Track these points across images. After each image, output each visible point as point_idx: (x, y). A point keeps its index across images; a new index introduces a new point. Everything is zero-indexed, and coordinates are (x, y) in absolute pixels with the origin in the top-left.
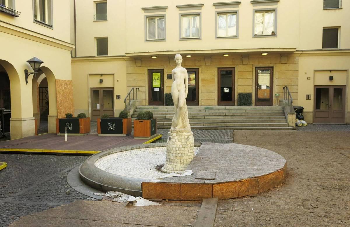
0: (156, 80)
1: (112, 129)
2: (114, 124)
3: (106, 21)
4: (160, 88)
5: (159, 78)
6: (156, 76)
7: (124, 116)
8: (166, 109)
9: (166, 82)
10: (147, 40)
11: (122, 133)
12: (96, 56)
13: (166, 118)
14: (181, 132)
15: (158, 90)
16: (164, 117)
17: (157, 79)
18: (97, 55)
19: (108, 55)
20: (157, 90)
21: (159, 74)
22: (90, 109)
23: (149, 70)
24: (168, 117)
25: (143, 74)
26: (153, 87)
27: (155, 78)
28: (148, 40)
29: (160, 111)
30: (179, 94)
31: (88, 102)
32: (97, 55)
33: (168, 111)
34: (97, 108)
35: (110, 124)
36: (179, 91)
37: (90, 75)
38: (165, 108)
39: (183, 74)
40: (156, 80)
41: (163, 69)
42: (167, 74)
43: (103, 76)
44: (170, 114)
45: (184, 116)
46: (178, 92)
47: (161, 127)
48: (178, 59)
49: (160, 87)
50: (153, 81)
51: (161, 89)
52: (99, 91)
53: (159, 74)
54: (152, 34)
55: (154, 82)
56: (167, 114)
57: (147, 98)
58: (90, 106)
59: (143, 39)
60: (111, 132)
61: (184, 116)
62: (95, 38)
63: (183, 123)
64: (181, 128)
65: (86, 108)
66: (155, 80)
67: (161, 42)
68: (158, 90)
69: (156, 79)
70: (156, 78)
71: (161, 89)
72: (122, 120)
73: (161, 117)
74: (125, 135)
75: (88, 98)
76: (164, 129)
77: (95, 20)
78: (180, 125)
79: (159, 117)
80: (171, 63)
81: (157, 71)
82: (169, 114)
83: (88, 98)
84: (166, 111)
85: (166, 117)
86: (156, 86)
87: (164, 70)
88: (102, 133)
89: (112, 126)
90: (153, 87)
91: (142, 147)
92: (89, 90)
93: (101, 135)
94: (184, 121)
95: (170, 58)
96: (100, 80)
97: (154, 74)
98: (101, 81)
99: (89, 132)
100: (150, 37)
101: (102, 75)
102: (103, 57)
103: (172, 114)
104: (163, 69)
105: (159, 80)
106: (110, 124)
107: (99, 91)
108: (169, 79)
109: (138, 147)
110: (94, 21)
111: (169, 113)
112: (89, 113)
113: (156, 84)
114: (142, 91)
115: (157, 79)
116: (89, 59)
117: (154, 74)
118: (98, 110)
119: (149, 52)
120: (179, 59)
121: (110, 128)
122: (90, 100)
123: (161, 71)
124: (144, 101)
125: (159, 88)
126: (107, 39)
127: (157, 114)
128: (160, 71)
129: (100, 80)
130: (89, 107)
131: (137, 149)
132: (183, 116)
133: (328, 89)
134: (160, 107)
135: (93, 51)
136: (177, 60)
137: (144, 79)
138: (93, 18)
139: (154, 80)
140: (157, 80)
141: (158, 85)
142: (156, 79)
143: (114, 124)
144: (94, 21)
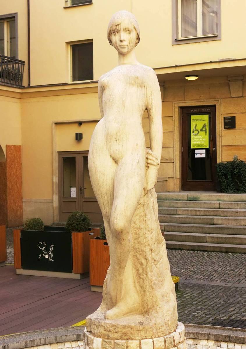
0: (199, 132)
1: (48, 259)
2: (52, 246)
3: (91, 4)
4: (207, 150)
5: (205, 126)
6: (199, 122)
7: (77, 225)
8: (218, 200)
9: (221, 136)
10: (177, 41)
11: (70, 272)
12: (69, 80)
13: (213, 224)
14: (125, 334)
15: (204, 156)
16: (209, 221)
17: (201, 130)
18: (73, 81)
19: (93, 79)
20: (200, 154)
21: (206, 117)
22: (56, 198)
23: (182, 108)
24: (220, 222)
25: (169, 119)
26: (192, 147)
27: (196, 126)
28: (180, 39)
29: (202, 206)
30: (116, 173)
31: (53, 182)
32: (73, 81)
33: (222, 206)
34: (71, 197)
35: (42, 245)
36: (116, 161)
37: (57, 124)
38: (215, 199)
39: (134, 90)
40: (199, 132)
41: (214, 106)
42: (224, 117)
43: (83, 126)
44: (225, 214)
45: (144, 261)
46: (114, 164)
47: (198, 246)
48: (118, 31)
49: (208, 147)
50: (192, 134)
51: (211, 152)
52: (75, 158)
53: (206, 117)
54: (189, 22)
55: (193, 137)
56: (218, 214)
57: (178, 175)
58: (56, 190)
59: (169, 38)
60: (44, 265)
61: (144, 261)
62: (68, 43)
63: (142, 291)
64: (131, 312)
65: (48, 197)
66: (196, 132)
67: (210, 43)
68: (204, 156)
69: (199, 130)
70: (199, 127)
71: (211, 152)
72: (70, 235)
73: (203, 221)
74: (78, 276)
75: (52, 175)
76: (206, 251)
77: (69, 4)
78: (131, 297)
79: (197, 221)
80: (232, 91)
81: (199, 110)
82: (222, 215)
83: (52, 175)
84: (218, 206)
85: (215, 222)
86: (198, 145)
87: (217, 107)
88: (24, 268)
89: (48, 250)
90: (192, 147)
91: (64, 338)
92: (56, 157)
93: (21, 271)
94: (146, 283)
95: (229, 79)
96: (77, 134)
97: (193, 117)
98: (79, 137)
99: (4, 262)
100: (185, 31)
101: (80, 123)
102: (84, 84)
103: (229, 214)
104: (214, 106)
105: (206, 132)
106: (42, 245)
107: (75, 158)
108: (229, 128)
109: (52, 340)
110: (65, 8)
111: (223, 211)
112: (53, 207)
113: (200, 141)
114: (167, 158)
115: (201, 130)
116: (55, 90)
117: (193, 117)
118: (73, 201)
119: (176, 66)
120: (122, 27)
121: (43, 255)
122: (56, 179)
123: (210, 111)
124: (169, 180)
125: (205, 150)
126: (91, 44)
127: (194, 213)
128: (208, 110)
129: (77, 134)
130: (53, 194)
131: (45, 344)
132: (142, 264)
133: (74, 158)
134: (204, 196)
135: (62, 69)
136: (114, 32)
137: (172, 130)
138: (64, 2)
139: (193, 132)
140: (201, 133)
141: (203, 143)
142: (199, 130)
143: (52, 246)
144: (65, 8)
